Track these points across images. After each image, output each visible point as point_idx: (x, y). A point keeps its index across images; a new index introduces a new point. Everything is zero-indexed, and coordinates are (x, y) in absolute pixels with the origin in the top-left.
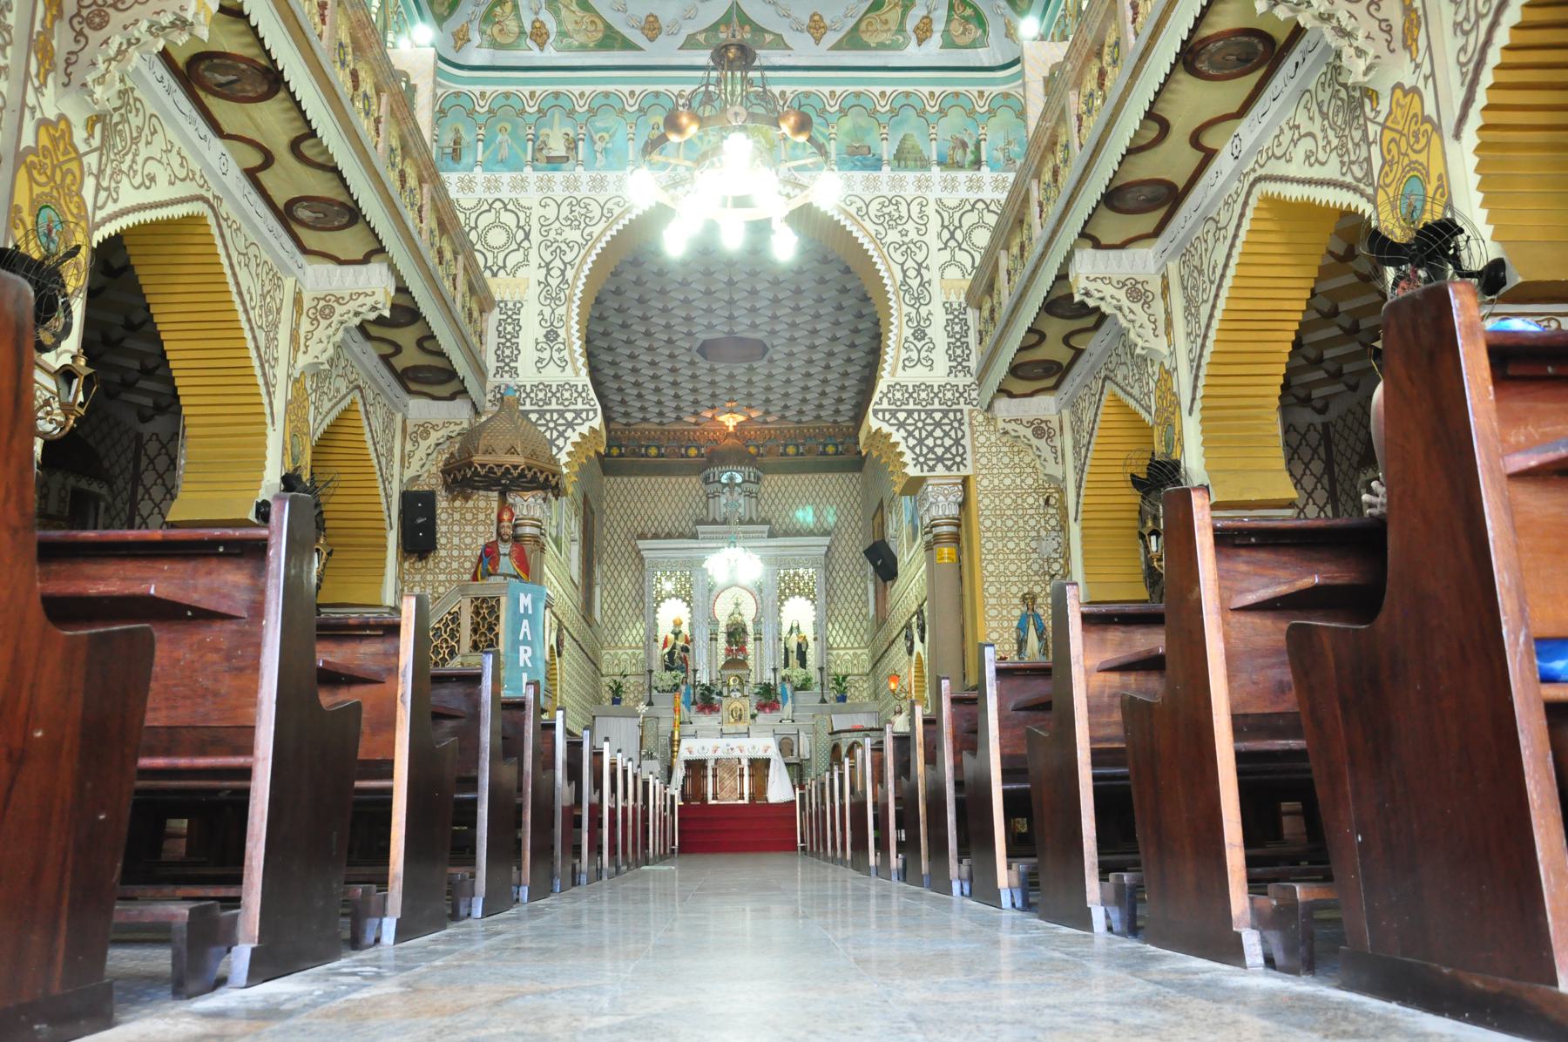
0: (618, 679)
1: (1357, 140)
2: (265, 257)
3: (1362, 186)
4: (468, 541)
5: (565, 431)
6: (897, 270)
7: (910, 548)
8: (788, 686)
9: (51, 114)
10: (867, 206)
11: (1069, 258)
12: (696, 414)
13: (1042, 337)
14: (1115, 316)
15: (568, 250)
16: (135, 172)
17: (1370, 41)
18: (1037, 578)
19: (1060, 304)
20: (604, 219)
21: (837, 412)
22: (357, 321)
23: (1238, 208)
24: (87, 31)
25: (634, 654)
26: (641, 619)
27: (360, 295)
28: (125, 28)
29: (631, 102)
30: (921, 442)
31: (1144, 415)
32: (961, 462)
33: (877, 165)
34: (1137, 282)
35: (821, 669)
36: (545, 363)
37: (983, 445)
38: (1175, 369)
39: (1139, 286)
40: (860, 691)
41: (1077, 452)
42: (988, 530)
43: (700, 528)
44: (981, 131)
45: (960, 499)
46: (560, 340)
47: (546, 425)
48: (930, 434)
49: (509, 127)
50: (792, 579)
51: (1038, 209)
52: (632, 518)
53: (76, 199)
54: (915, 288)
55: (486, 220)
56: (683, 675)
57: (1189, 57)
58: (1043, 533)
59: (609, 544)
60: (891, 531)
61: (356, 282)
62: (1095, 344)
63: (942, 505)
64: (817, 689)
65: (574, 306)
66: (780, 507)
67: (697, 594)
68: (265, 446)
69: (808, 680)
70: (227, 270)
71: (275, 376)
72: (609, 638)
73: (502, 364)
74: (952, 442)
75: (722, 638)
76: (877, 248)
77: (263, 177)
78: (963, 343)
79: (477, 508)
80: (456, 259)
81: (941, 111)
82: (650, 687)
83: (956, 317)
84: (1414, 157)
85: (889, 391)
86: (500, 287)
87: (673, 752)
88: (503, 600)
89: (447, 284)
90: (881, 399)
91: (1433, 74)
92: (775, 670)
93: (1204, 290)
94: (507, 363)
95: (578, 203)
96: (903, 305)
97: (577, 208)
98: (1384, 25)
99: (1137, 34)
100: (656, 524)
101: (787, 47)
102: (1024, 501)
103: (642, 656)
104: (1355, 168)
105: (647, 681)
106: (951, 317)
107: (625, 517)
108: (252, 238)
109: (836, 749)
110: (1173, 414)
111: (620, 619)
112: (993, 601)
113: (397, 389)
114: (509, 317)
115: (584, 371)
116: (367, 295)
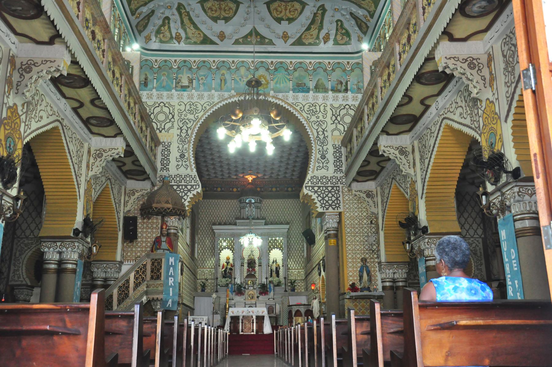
0: (203, 281)
1: (476, 113)
2: (78, 137)
3: (477, 130)
4: (149, 235)
5: (187, 193)
6: (315, 132)
7: (320, 234)
8: (272, 285)
9: (11, 105)
10: (304, 107)
11: (378, 138)
12: (236, 175)
13: (369, 163)
14: (394, 160)
15: (189, 122)
16: (36, 116)
17: (477, 84)
18: (367, 252)
19: (374, 152)
20: (203, 111)
21: (293, 175)
22: (111, 158)
23: (438, 126)
24: (24, 74)
25: (210, 271)
26: (213, 256)
27: (113, 149)
28: (38, 73)
29: (214, 65)
30: (323, 199)
31: (406, 195)
32: (339, 207)
33: (308, 91)
34: (403, 148)
35: (285, 278)
36: (180, 166)
37: (347, 200)
38: (416, 181)
39: (404, 149)
40: (300, 286)
41: (382, 204)
42: (349, 233)
43: (238, 221)
44: (348, 78)
45: (338, 221)
46: (185, 157)
47: (180, 191)
48: (327, 196)
49: (166, 73)
50: (274, 242)
51: (367, 117)
52: (210, 216)
53: (18, 132)
54: (322, 139)
55: (157, 110)
56: (230, 280)
57: (418, 78)
58: (370, 234)
59: (201, 221)
60: (313, 225)
61: (111, 144)
62: (389, 166)
63: (331, 223)
64: (283, 286)
65: (191, 145)
66: (269, 212)
67: (235, 248)
68: (76, 207)
69: (280, 282)
70: (65, 145)
71: (81, 181)
72: (201, 264)
73: (163, 167)
74: (335, 199)
75: (246, 265)
76: (307, 123)
77: (80, 111)
78: (340, 160)
79: (153, 222)
80: (147, 129)
81: (332, 69)
82: (217, 284)
83: (337, 150)
84: (493, 126)
85: (311, 179)
86: (162, 137)
87: (226, 312)
88: (163, 260)
89: (144, 140)
90: (308, 182)
91: (498, 98)
92: (267, 278)
93: (427, 154)
94: (165, 167)
95: (193, 104)
96: (317, 146)
97: (192, 106)
98: (483, 78)
99: (401, 65)
100: (220, 218)
101: (274, 44)
102: (363, 222)
103: (214, 272)
104: (475, 123)
105: (215, 282)
106: (335, 150)
107: (208, 216)
108: (74, 131)
109: (290, 312)
110: (416, 197)
111: (205, 257)
112: (350, 260)
113: (123, 177)
114: (166, 148)
115: (195, 170)
116: (115, 149)
